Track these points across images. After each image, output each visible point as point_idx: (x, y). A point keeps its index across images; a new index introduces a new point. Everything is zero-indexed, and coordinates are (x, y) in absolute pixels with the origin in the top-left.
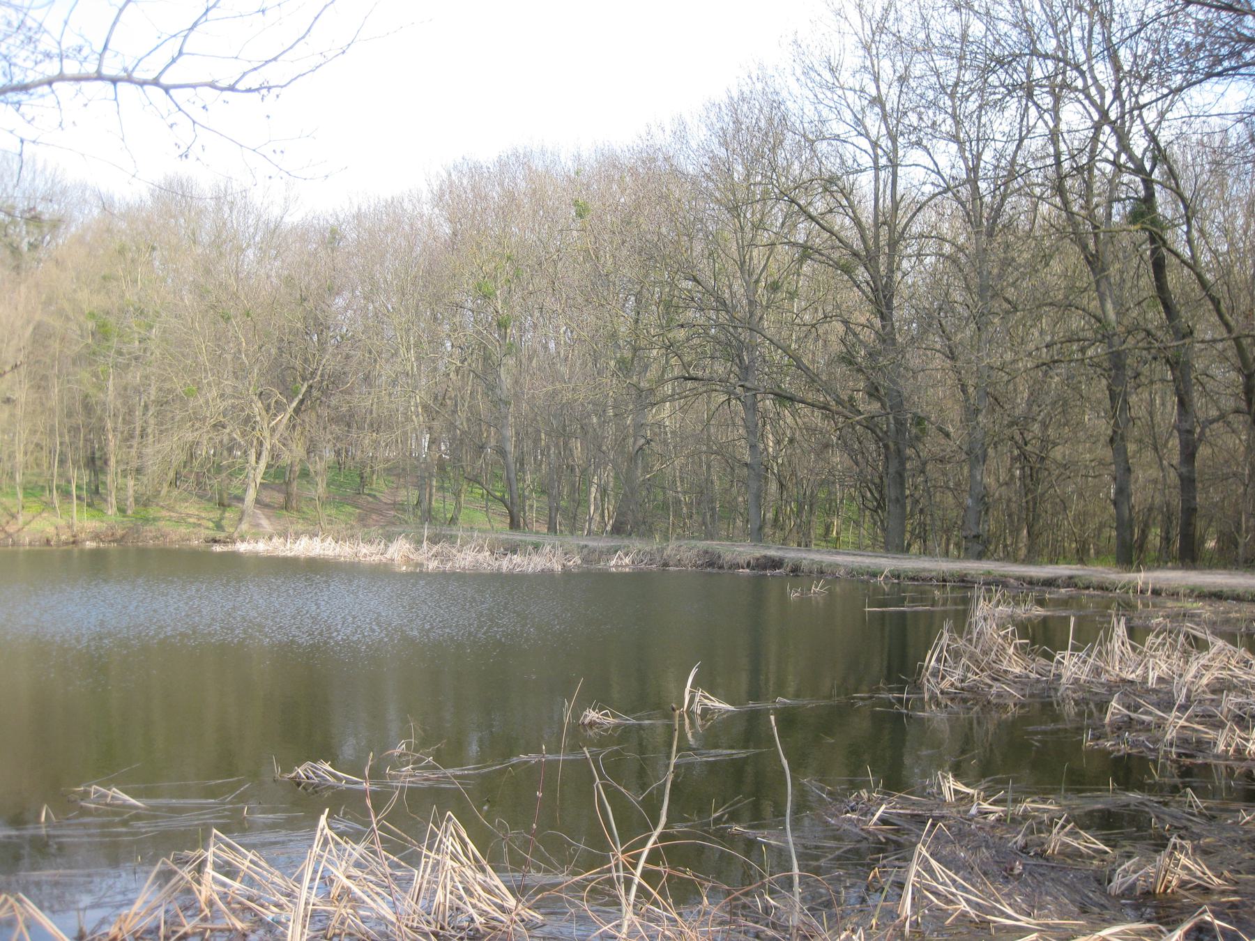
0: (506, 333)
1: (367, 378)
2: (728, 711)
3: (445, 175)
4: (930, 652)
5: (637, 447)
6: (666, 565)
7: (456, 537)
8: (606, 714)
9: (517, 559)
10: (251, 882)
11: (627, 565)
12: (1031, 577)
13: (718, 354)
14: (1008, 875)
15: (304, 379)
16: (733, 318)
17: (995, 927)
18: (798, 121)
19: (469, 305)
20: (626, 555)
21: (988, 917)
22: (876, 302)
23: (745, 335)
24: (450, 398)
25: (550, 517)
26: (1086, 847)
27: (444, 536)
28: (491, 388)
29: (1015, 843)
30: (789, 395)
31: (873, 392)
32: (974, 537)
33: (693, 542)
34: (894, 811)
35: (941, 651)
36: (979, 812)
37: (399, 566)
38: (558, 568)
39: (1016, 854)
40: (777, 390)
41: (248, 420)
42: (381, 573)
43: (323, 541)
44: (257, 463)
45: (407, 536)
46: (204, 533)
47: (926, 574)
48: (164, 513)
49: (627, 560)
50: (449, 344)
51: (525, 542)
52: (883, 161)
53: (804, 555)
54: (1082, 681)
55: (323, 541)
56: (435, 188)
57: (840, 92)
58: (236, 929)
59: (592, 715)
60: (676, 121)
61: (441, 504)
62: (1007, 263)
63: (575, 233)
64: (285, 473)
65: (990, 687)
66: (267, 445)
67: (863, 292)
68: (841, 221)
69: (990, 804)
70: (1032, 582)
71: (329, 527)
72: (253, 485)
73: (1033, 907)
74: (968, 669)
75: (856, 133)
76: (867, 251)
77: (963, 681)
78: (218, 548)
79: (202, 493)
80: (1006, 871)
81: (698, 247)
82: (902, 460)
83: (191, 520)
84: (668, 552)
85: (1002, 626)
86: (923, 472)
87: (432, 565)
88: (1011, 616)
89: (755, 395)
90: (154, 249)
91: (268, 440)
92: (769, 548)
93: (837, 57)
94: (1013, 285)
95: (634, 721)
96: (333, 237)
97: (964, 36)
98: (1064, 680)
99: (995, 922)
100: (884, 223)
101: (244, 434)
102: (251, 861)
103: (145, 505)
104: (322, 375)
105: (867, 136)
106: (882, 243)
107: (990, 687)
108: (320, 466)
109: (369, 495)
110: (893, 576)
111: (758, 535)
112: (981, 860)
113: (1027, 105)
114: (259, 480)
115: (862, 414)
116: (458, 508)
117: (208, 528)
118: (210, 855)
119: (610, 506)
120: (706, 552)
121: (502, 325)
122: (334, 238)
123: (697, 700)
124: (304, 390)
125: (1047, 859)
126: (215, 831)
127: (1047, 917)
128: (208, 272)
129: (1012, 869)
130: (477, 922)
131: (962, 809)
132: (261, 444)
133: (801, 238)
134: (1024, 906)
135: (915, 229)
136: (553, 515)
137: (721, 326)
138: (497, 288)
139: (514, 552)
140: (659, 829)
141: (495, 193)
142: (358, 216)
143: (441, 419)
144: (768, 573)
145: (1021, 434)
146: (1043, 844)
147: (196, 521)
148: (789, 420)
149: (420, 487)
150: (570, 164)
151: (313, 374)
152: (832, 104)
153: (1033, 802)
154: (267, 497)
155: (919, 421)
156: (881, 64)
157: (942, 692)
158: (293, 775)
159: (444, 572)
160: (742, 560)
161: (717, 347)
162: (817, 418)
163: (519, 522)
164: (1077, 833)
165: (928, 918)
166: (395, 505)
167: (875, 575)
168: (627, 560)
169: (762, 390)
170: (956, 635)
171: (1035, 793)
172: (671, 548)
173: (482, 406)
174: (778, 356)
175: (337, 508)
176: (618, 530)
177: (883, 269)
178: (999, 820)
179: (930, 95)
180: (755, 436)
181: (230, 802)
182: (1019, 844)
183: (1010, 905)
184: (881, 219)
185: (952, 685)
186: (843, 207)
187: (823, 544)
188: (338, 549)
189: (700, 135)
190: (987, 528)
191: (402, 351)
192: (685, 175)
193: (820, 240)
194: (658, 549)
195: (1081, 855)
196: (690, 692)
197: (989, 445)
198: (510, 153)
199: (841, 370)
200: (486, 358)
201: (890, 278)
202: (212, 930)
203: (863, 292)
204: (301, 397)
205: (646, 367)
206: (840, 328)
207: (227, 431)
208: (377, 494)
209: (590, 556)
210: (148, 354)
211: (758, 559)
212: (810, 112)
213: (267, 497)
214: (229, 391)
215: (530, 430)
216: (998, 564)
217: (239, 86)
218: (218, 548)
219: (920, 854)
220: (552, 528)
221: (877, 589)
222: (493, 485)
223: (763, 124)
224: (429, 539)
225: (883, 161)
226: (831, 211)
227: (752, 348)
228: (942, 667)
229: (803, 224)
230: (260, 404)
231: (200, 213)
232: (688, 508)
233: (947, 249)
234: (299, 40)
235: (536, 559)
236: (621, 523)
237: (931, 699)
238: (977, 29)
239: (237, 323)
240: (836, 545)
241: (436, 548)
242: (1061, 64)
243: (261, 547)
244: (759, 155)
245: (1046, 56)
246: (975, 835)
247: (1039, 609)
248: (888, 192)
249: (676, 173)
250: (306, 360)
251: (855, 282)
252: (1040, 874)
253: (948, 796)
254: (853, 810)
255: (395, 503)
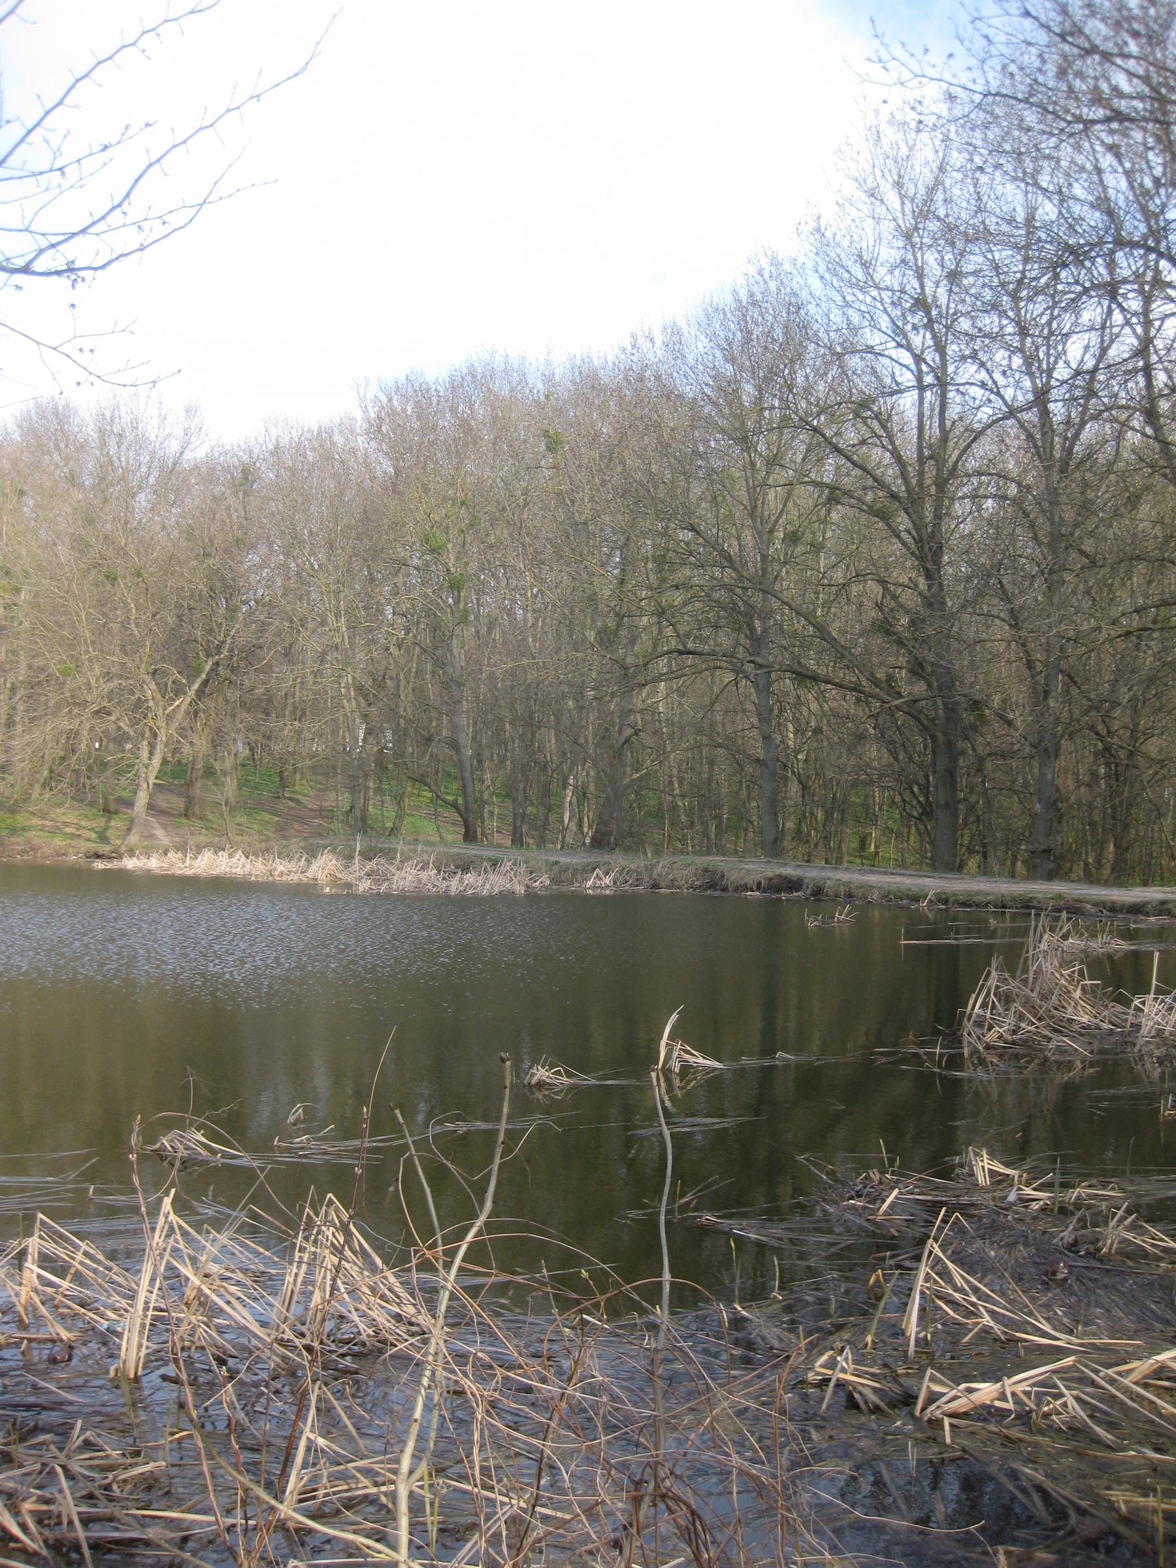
0: (459, 596)
1: (287, 654)
2: (716, 1069)
3: (384, 399)
4: (974, 996)
5: (622, 740)
6: (656, 886)
7: (395, 851)
8: (558, 1073)
9: (470, 878)
10: (79, 1278)
11: (607, 887)
12: (1113, 902)
13: (722, 622)
14: (1048, 1280)
15: (208, 655)
16: (741, 578)
17: (1023, 1347)
18: (822, 330)
19: (416, 562)
20: (606, 873)
21: (1017, 1334)
22: (921, 558)
23: (757, 599)
24: (391, 678)
25: (515, 827)
26: (1153, 1245)
27: (382, 850)
28: (440, 664)
29: (1062, 1239)
30: (810, 673)
31: (917, 669)
32: (1044, 851)
33: (691, 858)
34: (911, 1197)
35: (988, 995)
36: (1020, 1199)
37: (322, 889)
38: (520, 890)
39: (1061, 1252)
40: (796, 667)
41: (139, 704)
42: (305, 892)
43: (231, 856)
44: (150, 759)
45: (333, 851)
46: (84, 846)
47: (981, 898)
48: (36, 821)
49: (607, 881)
50: (389, 610)
51: (482, 857)
52: (929, 379)
53: (829, 874)
54: (1167, 1034)
55: (231, 856)
56: (372, 415)
57: (874, 293)
58: (61, 1340)
59: (542, 1073)
60: (669, 330)
61: (381, 810)
62: (1085, 508)
63: (547, 473)
64: (186, 771)
65: (1049, 1039)
66: (162, 737)
67: (904, 544)
68: (878, 456)
69: (1034, 1189)
70: (1114, 908)
71: (239, 838)
72: (145, 785)
73: (1078, 1322)
74: (1021, 1017)
75: (893, 344)
76: (908, 491)
77: (1014, 1032)
78: (99, 865)
79: (79, 794)
80: (1046, 1275)
81: (697, 489)
82: (954, 755)
83: (68, 830)
84: (659, 869)
85: (1064, 964)
86: (980, 770)
87: (364, 886)
88: (1084, 951)
89: (769, 673)
90: (22, 493)
91: (163, 731)
92: (785, 865)
93: (871, 248)
94: (1092, 534)
95: (594, 1082)
96: (245, 477)
97: (1030, 219)
98: (1144, 1031)
99: (1026, 1341)
100: (931, 457)
101: (134, 722)
102: (86, 1254)
103: (12, 812)
104: (231, 650)
105: (909, 348)
106: (928, 482)
107: (1049, 1039)
108: (228, 763)
109: (290, 799)
110: (940, 901)
111: (774, 848)
112: (1017, 1260)
113: (1109, 307)
114: (152, 780)
115: (902, 697)
116: (400, 817)
117: (89, 840)
118: (34, 1244)
119: (589, 814)
120: (706, 870)
121: (455, 586)
122: (246, 479)
123: (675, 1054)
124: (208, 668)
125: (1101, 1261)
126: (40, 1216)
127: (1094, 1334)
128: (90, 521)
129: (1054, 1273)
130: (364, 1334)
131: (998, 1194)
132: (155, 735)
133: (828, 478)
134: (1066, 1320)
135: (971, 464)
136: (518, 824)
137: (729, 588)
138: (448, 541)
139: (466, 869)
140: (483, 1218)
141: (446, 421)
142: (277, 451)
143: (380, 704)
144: (783, 896)
145: (1104, 722)
146: (1098, 1240)
147: (74, 831)
148: (814, 706)
149: (352, 790)
150: (540, 385)
151: (219, 649)
152: (864, 308)
153: (1090, 1186)
154: (163, 801)
155: (976, 705)
156: (926, 257)
157: (988, 1047)
158: (156, 1147)
159: (378, 894)
160: (750, 880)
161: (722, 613)
162: (847, 703)
163: (475, 832)
164: (1141, 1227)
165: (943, 1336)
166: (321, 812)
167: (916, 899)
168: (607, 881)
169: (777, 667)
170: (1007, 975)
171: (1090, 1175)
172: (662, 866)
173: (433, 690)
174: (799, 624)
175: (249, 815)
176: (599, 842)
177: (929, 515)
178: (1043, 1209)
179: (988, 295)
180: (770, 726)
181: (72, 1182)
182: (1065, 1241)
183: (1047, 1319)
184: (926, 453)
185: (1001, 1037)
186: (879, 437)
187: (858, 861)
188: (248, 866)
189: (699, 346)
190: (1060, 840)
191: (331, 618)
192: (680, 397)
193: (851, 479)
194: (646, 866)
195: (1146, 1255)
196: (667, 1044)
197: (1062, 736)
198: (465, 371)
199: (878, 641)
200: (435, 628)
201: (937, 525)
202: (30, 1340)
203: (904, 544)
204: (204, 676)
205: (633, 641)
206: (875, 589)
207: (113, 718)
208: (300, 797)
209: (561, 875)
210: (16, 624)
211: (771, 879)
212: (837, 318)
213: (163, 801)
214: (115, 670)
215: (490, 717)
216: (1072, 885)
217: (38, 266)
218: (99, 865)
219: (931, 1252)
220: (518, 841)
221: (919, 918)
222: (446, 787)
223: (778, 333)
224: (361, 853)
225: (929, 379)
226: (863, 442)
227: (766, 615)
228: (988, 1015)
229: (831, 461)
230: (153, 686)
231: (82, 447)
232: (687, 816)
233: (1013, 490)
234: (114, 208)
235: (494, 878)
236: (603, 834)
237: (971, 1056)
238: (1048, 210)
239: (125, 584)
240: (872, 862)
241: (370, 865)
242: (1153, 256)
243: (154, 863)
244: (773, 372)
245: (1134, 245)
246: (1010, 1228)
247: (1120, 942)
248: (936, 419)
249: (670, 395)
250: (211, 631)
251: (893, 531)
252: (1090, 1280)
253: (982, 1179)
254: (859, 1195)
255: (321, 810)
